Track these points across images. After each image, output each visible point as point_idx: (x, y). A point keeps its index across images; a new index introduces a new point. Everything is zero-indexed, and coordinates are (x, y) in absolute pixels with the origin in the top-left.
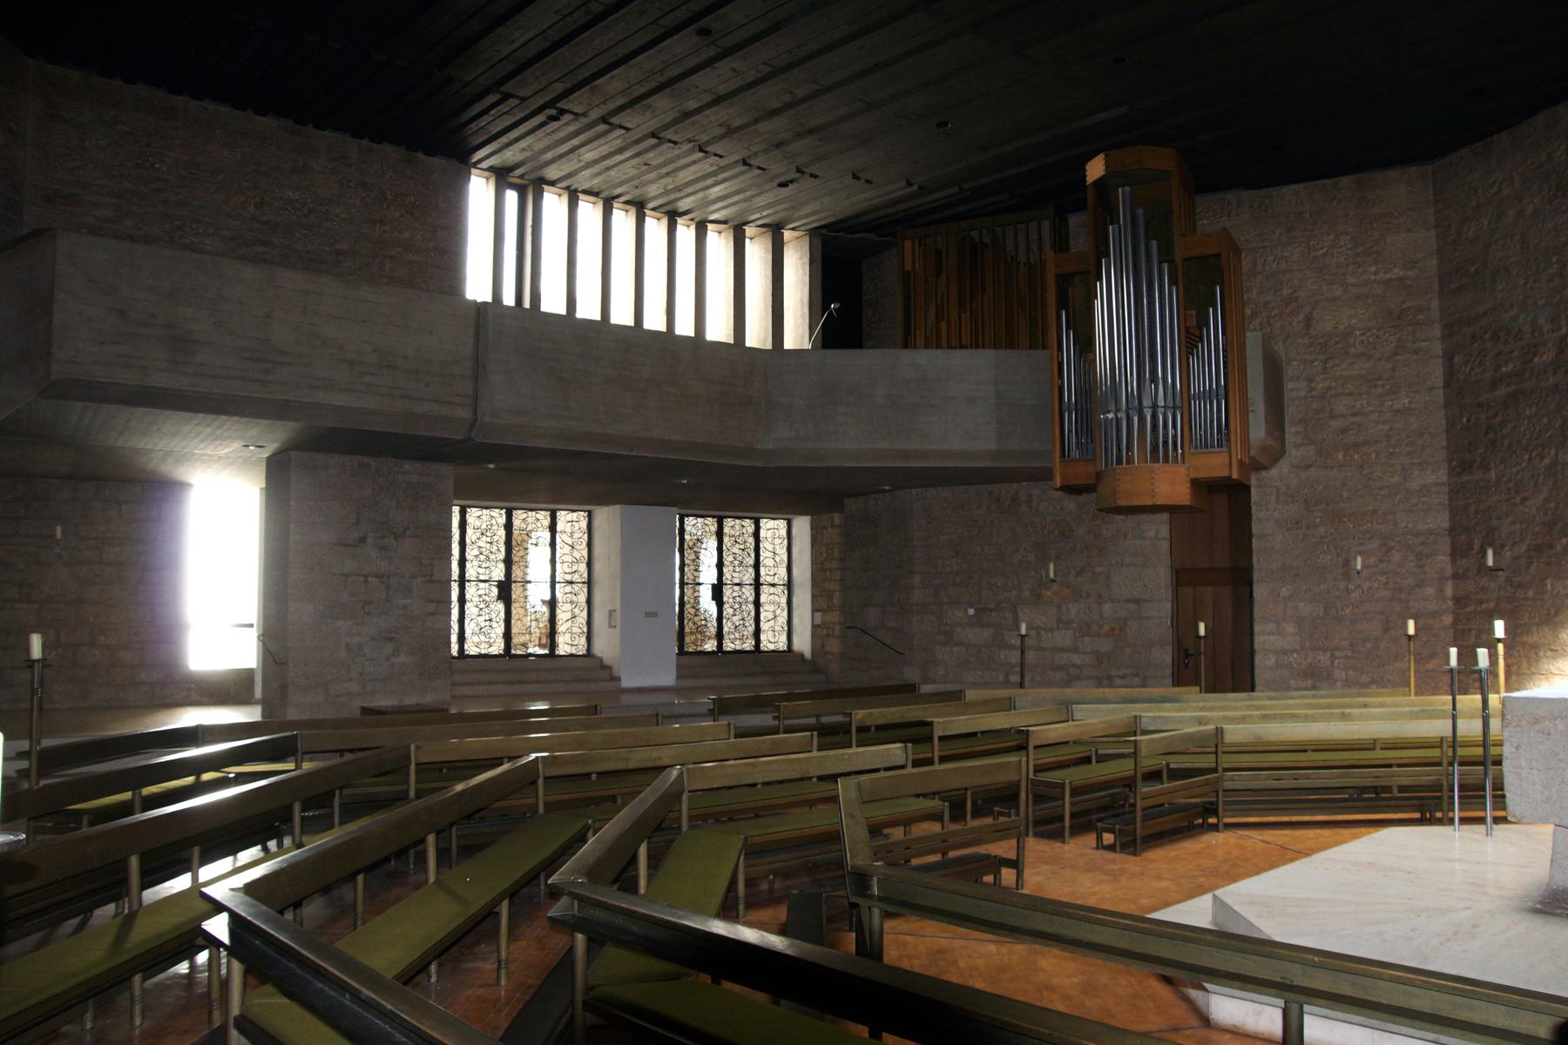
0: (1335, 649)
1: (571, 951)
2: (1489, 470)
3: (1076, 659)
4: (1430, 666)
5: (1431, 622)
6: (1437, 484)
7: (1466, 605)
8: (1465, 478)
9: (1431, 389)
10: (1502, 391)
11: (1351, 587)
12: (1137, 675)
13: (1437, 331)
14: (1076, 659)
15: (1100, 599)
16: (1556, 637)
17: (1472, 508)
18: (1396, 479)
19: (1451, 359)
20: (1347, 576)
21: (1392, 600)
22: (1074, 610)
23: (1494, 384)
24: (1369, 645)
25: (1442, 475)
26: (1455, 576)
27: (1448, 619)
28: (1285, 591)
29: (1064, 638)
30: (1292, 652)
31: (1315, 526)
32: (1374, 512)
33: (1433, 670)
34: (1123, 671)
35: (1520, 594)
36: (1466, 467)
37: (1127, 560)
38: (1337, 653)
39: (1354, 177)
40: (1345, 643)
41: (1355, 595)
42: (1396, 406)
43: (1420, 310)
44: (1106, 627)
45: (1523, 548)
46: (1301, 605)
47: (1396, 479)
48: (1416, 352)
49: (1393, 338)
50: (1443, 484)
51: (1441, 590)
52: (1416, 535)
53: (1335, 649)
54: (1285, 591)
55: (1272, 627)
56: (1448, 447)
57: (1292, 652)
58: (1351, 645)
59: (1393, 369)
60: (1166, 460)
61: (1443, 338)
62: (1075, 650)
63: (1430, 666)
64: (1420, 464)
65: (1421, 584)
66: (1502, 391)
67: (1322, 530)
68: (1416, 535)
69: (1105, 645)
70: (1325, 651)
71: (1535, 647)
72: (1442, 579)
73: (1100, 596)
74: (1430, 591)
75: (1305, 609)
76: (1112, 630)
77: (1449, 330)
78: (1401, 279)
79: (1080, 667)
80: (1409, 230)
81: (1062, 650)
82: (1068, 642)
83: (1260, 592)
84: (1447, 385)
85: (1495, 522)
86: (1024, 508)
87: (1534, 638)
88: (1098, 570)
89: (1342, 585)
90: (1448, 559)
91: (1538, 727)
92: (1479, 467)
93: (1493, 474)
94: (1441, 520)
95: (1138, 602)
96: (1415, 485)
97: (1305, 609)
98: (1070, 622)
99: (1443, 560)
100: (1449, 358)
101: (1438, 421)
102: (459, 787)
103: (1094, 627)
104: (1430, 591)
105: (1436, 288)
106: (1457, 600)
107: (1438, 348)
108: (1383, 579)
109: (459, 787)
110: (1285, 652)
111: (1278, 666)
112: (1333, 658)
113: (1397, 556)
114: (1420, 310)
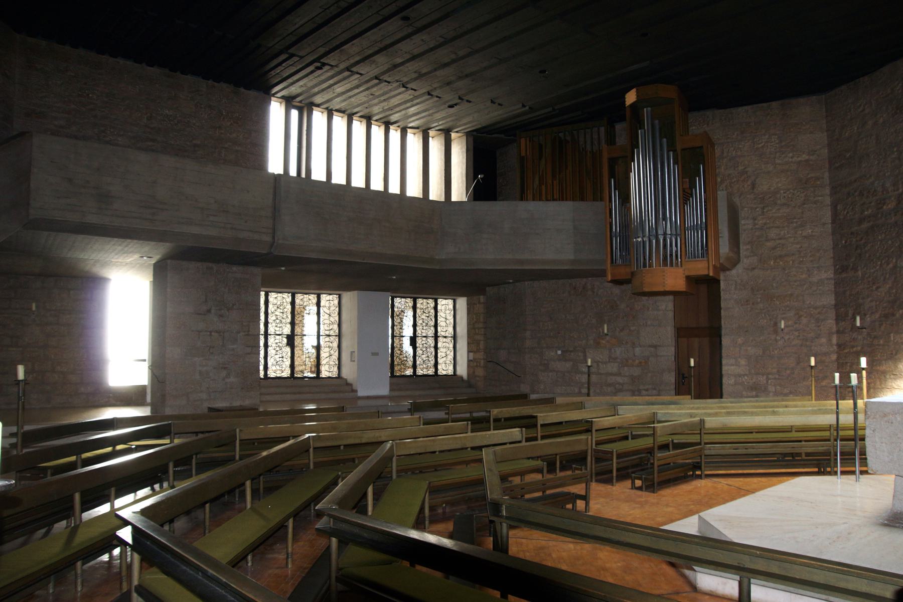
0: (769, 374)
1: (329, 548)
2: (857, 271)
3: (619, 379)
4: (824, 384)
5: (824, 358)
6: (827, 279)
7: (844, 349)
8: (844, 275)
9: (824, 224)
10: (865, 225)
11: (778, 338)
12: (655, 389)
13: (827, 191)
14: (619, 379)
15: (634, 345)
16: (896, 367)
17: (848, 293)
18: (804, 276)
19: (836, 207)
20: (776, 332)
21: (801, 345)
22: (618, 352)
23: (861, 221)
24: (788, 372)
25: (830, 274)
26: (838, 332)
27: (834, 357)
28: (740, 341)
29: (613, 368)
30: (744, 375)
31: (758, 303)
32: (791, 295)
33: (825, 386)
34: (647, 387)
35: (876, 342)
36: (844, 269)
37: (649, 323)
38: (770, 376)
39: (780, 102)
40: (775, 371)
41: (781, 343)
42: (804, 234)
43: (818, 179)
44: (637, 361)
45: (877, 316)
46: (749, 348)
47: (804, 276)
48: (815, 203)
49: (802, 195)
50: (831, 279)
51: (830, 340)
52: (816, 308)
53: (769, 374)
54: (740, 341)
55: (732, 361)
56: (834, 258)
57: (744, 375)
58: (778, 371)
59: (802, 213)
60: (672, 265)
61: (831, 195)
62: (619, 374)
63: (824, 384)
64: (818, 267)
65: (818, 337)
66: (865, 225)
67: (761, 305)
68: (816, 308)
69: (636, 372)
70: (763, 375)
71: (884, 373)
72: (830, 334)
73: (634, 343)
74: (824, 340)
75: (752, 351)
76: (640, 363)
77: (834, 190)
78: (807, 161)
79: (622, 384)
80: (811, 133)
81: (612, 374)
82: (615, 370)
83: (726, 341)
84: (833, 222)
85: (861, 301)
86: (590, 293)
87: (883, 368)
88: (632, 328)
89: (773, 337)
90: (834, 322)
91: (886, 419)
92: (852, 269)
93: (860, 273)
94: (830, 300)
95: (655, 347)
96: (815, 279)
97: (752, 351)
98: (616, 358)
99: (831, 323)
100: (834, 206)
101: (828, 242)
102: (265, 454)
103: (630, 361)
104: (824, 340)
105: (827, 166)
106: (839, 346)
107: (828, 201)
108: (797, 333)
109: (265, 454)
110: (740, 376)
111: (736, 384)
112: (768, 379)
113: (804, 320)
114: (818, 179)
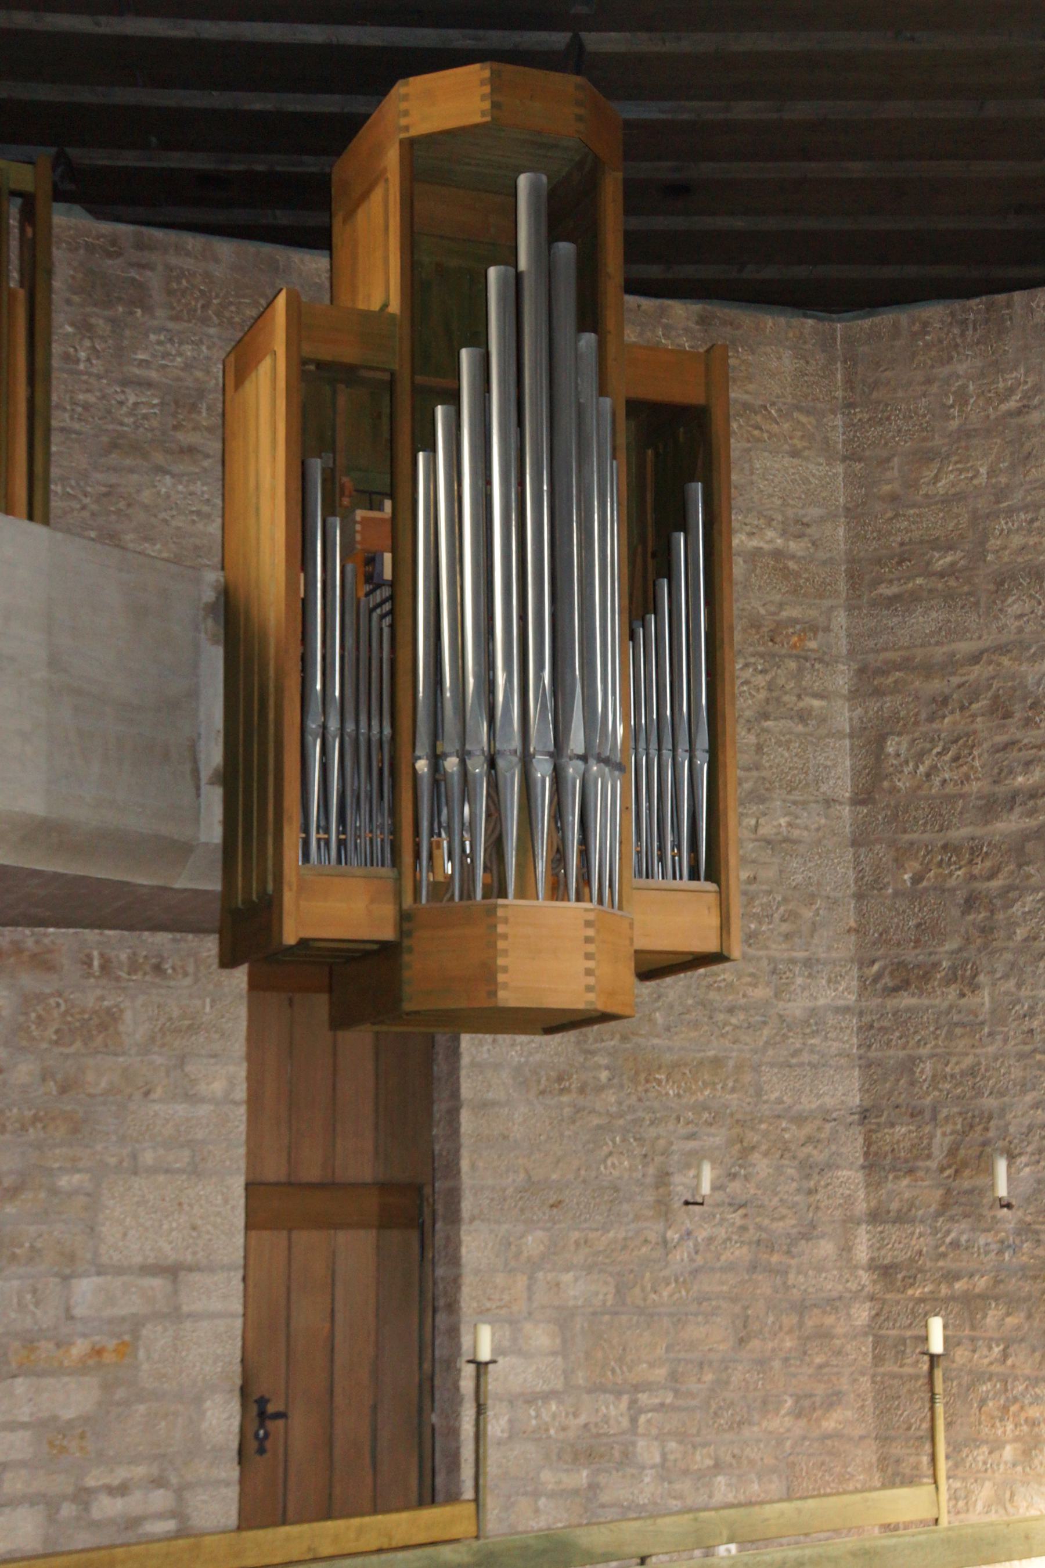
0: (637, 1388)
2: (975, 988)
4: (830, 1424)
5: (829, 1320)
6: (838, 1010)
7: (911, 1281)
8: (906, 1000)
9: (829, 802)
10: (1011, 824)
11: (673, 1235)
12: (159, 1482)
13: (841, 679)
15: (69, 1266)
17: (928, 1068)
18: (760, 993)
19: (881, 740)
20: (663, 1209)
21: (753, 1267)
23: (991, 807)
24: (709, 1377)
25: (845, 992)
26: (875, 1217)
27: (862, 1314)
28: (533, 1243)
30: (547, 1396)
31: (600, 1089)
32: (717, 1062)
33: (837, 1435)
34: (121, 1474)
36: (906, 978)
37: (148, 1157)
38: (643, 1398)
39: (696, 308)
40: (660, 1373)
41: (680, 1256)
42: (766, 830)
43: (812, 629)
44: (79, 1348)
46: (567, 1277)
47: (760, 993)
48: (803, 717)
49: (761, 680)
50: (847, 1009)
51: (846, 1248)
52: (800, 1120)
53: (637, 1388)
54: (533, 1243)
56: (858, 931)
57: (547, 1396)
58: (674, 1376)
59: (759, 748)
60: (372, 865)
61: (855, 695)
63: (830, 1424)
64: (808, 963)
65: (808, 1233)
66: (1011, 824)
67: (610, 1097)
68: (800, 1120)
69: (74, 1398)
70: (619, 1394)
72: (850, 1222)
73: (71, 1258)
74: (826, 1248)
75: (577, 1289)
76: (98, 1352)
77: (869, 681)
78: (778, 554)
80: (795, 454)
83: (476, 1246)
84: (862, 798)
85: (990, 1103)
88: (64, 1182)
89: (653, 1230)
90: (859, 1176)
92: (952, 978)
93: (985, 997)
94: (845, 1091)
95: (172, 1271)
96: (796, 1007)
97: (577, 1289)
99: (850, 1178)
100: (871, 741)
101: (840, 872)
102: (448, 695)
103: (46, 1347)
104: (826, 1248)
105: (842, 586)
107: (844, 716)
108: (736, 1218)
109: (448, 695)
112: (635, 1411)
113: (762, 1166)
114: (812, 629)
